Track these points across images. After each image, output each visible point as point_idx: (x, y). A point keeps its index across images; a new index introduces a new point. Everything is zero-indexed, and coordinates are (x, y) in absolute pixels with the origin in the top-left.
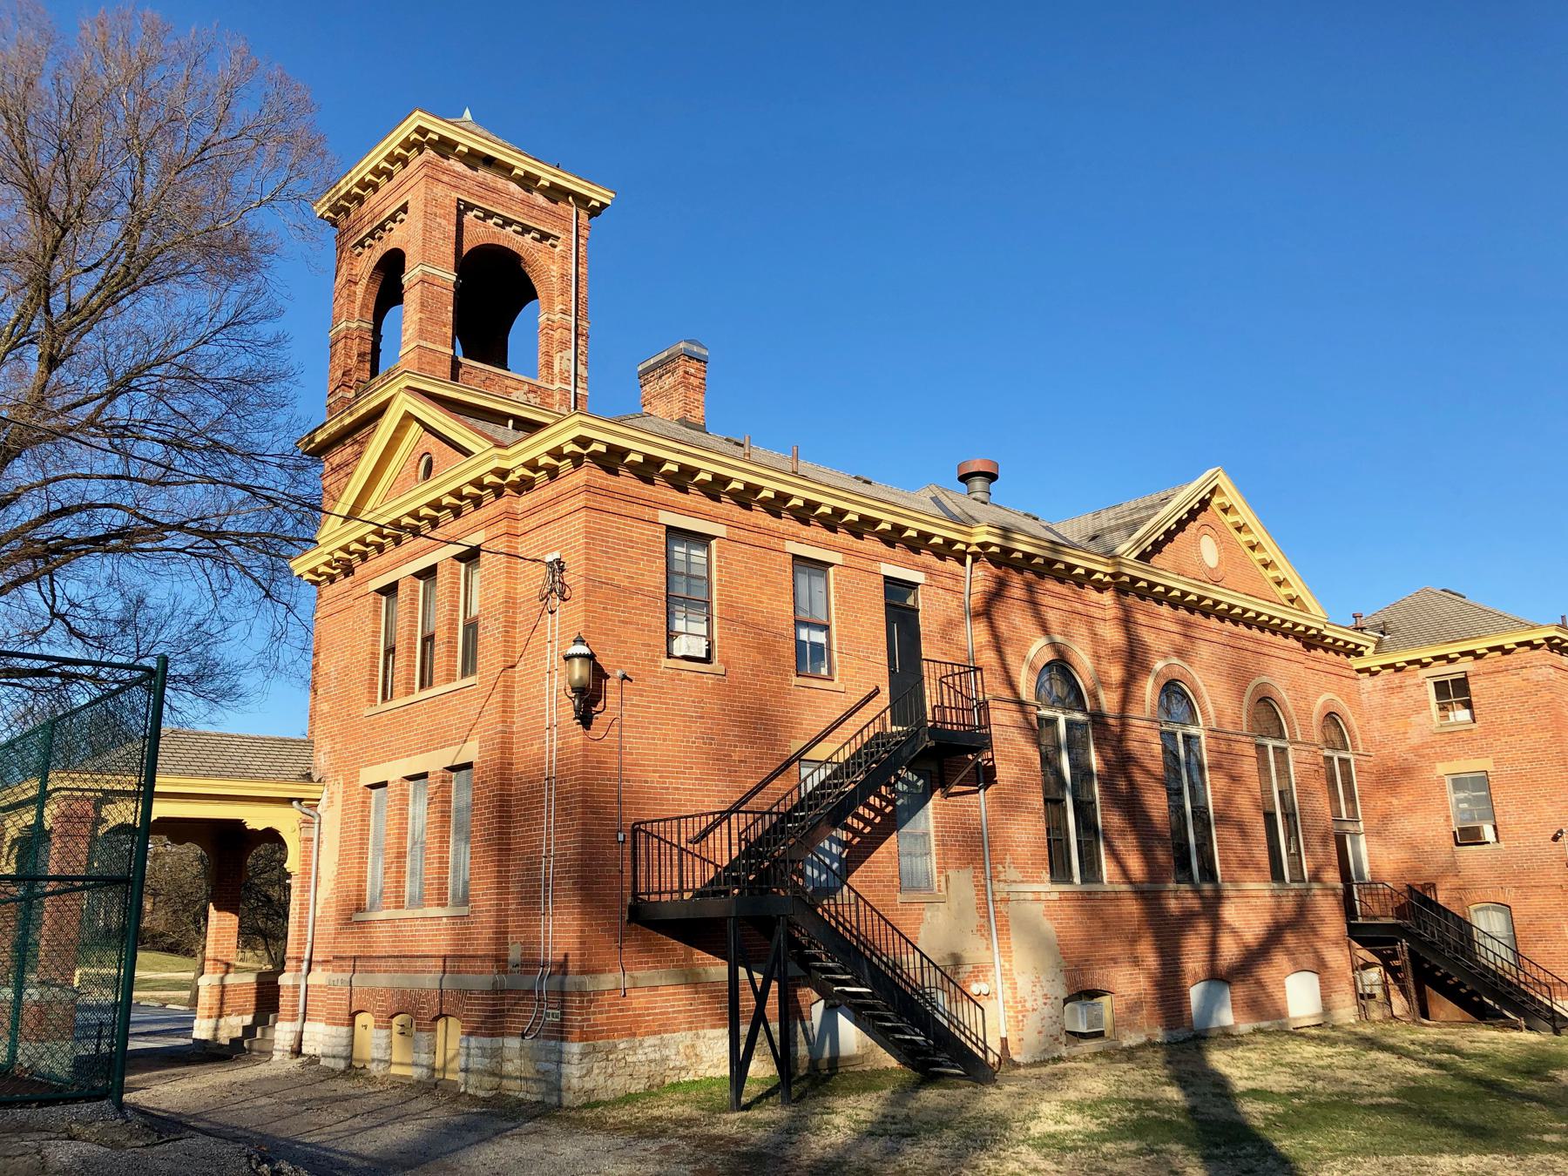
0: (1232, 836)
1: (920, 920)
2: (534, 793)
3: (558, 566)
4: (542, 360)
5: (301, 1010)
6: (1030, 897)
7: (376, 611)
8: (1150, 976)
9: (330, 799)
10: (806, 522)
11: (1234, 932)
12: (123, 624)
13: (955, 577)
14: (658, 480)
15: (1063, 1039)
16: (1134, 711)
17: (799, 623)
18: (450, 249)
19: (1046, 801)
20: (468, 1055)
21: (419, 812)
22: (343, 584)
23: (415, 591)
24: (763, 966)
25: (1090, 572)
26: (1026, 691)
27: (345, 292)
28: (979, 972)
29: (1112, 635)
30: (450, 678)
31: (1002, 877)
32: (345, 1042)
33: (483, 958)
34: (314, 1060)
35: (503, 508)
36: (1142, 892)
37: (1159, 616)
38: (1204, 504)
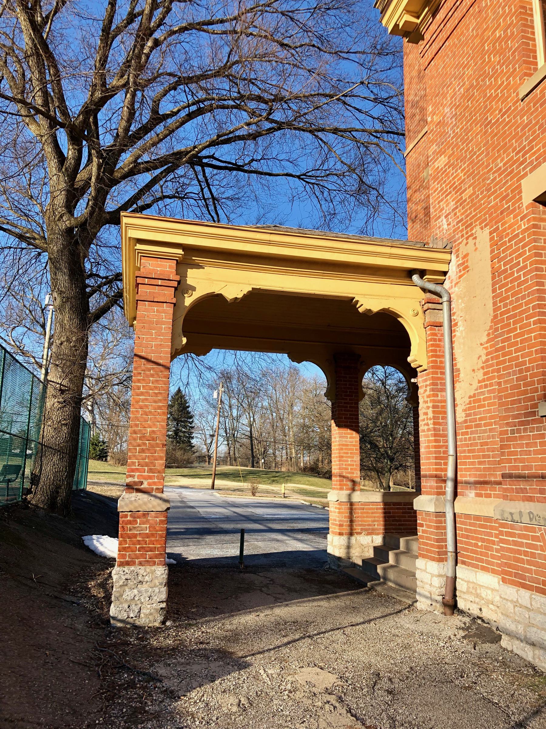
5: (450, 548)
9: (464, 267)
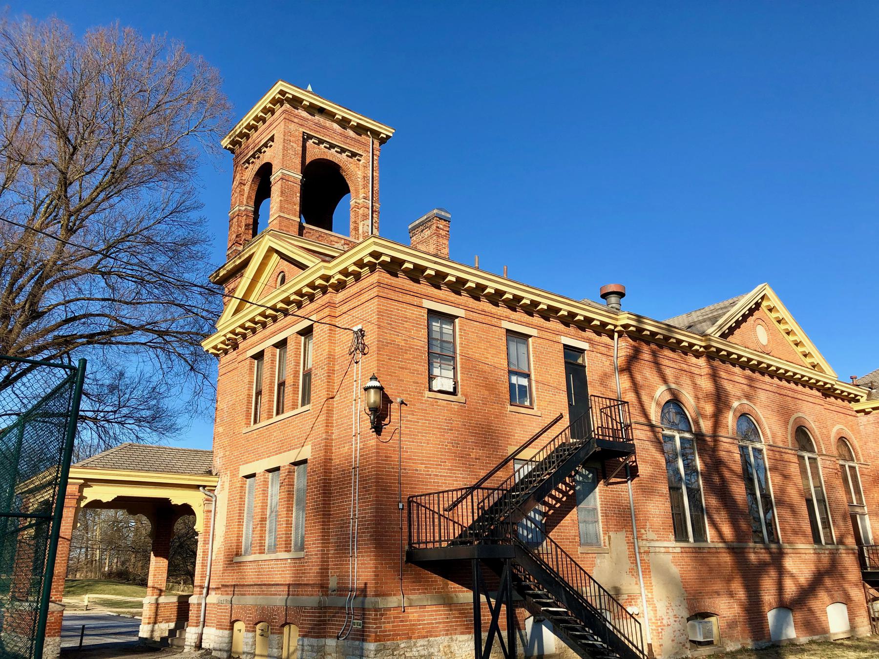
0: (787, 514)
1: (593, 565)
2: (345, 478)
3: (361, 333)
4: (352, 226)
5: (202, 619)
6: (663, 550)
7: (251, 369)
8: (741, 605)
10: (514, 310)
11: (792, 576)
12: (113, 388)
13: (607, 346)
14: (422, 281)
15: (688, 645)
16: (722, 432)
17: (511, 373)
18: (298, 161)
19: (670, 488)
20: (303, 650)
21: (275, 492)
22: (232, 355)
23: (274, 355)
24: (496, 593)
25: (691, 345)
26: (655, 415)
27: (238, 190)
28: (632, 599)
29: (706, 385)
30: (295, 406)
31: (644, 537)
32: (227, 640)
33: (312, 585)
34: (208, 652)
35: (327, 300)
36: (733, 548)
37: (734, 374)
38: (758, 305)
